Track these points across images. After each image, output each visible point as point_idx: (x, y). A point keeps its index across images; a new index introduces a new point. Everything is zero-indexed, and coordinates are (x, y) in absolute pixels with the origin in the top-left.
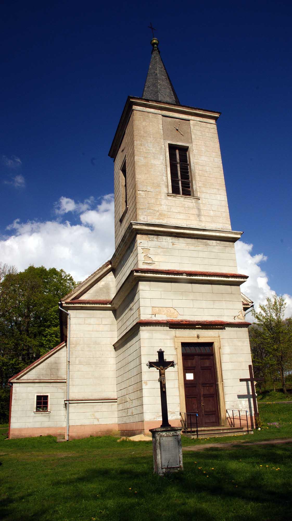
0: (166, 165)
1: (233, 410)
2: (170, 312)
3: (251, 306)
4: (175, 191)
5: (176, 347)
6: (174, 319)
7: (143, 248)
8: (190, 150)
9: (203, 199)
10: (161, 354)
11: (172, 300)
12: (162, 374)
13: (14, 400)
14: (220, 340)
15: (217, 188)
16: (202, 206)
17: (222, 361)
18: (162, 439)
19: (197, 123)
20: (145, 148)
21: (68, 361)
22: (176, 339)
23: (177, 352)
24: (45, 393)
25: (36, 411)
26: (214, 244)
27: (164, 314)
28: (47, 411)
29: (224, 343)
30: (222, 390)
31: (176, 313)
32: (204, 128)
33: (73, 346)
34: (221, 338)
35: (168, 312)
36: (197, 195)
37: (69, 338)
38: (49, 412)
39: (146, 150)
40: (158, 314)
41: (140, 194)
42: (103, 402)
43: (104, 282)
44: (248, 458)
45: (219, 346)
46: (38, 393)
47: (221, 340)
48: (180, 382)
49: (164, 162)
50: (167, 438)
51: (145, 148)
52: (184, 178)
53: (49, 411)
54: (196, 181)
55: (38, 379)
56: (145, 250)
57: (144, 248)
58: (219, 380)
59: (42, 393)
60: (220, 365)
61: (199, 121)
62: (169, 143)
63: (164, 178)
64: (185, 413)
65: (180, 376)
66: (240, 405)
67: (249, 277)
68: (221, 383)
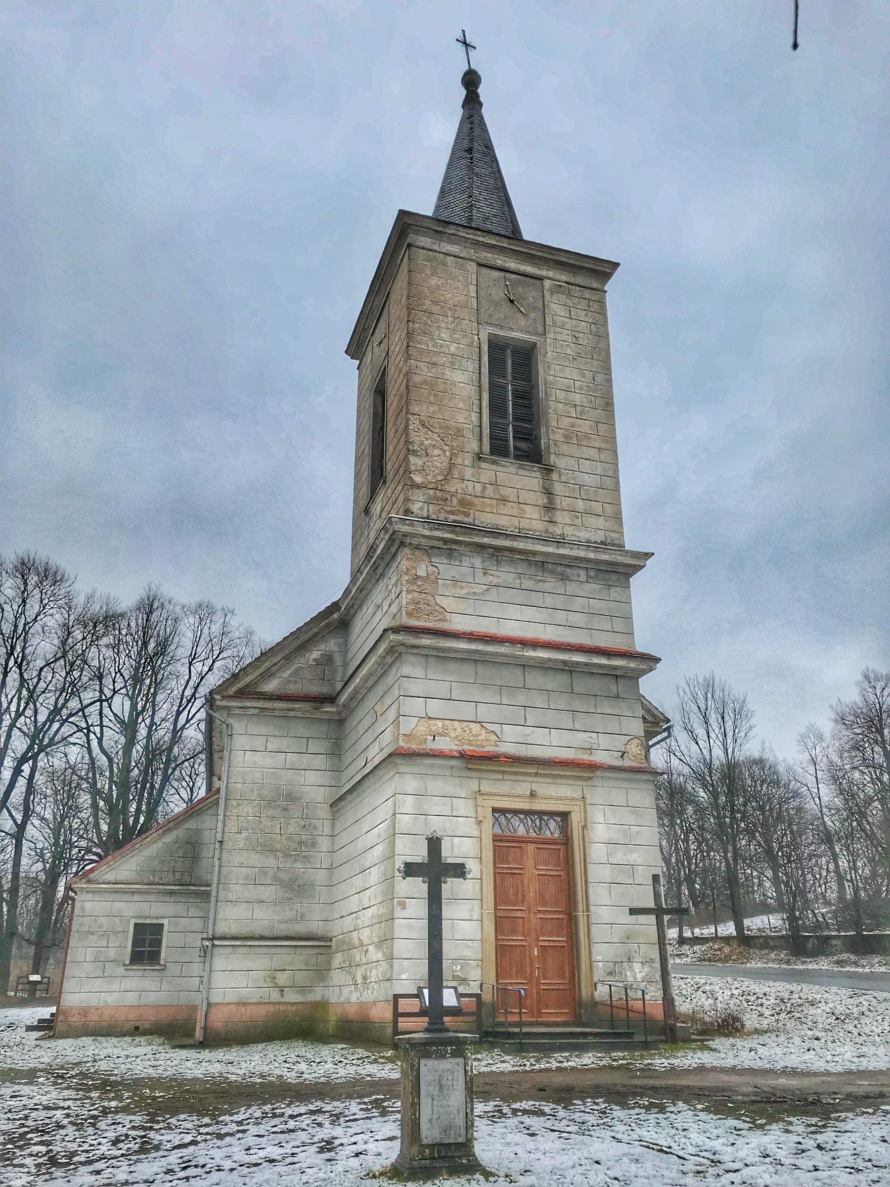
0: (480, 386)
1: (610, 986)
2: (471, 732)
3: (665, 730)
4: (499, 449)
5: (480, 818)
6: (478, 749)
8: (759, 930)
9: (562, 470)
10: (434, 844)
11: (501, 689)
12: (435, 901)
13: (76, 934)
14: (585, 807)
15: (596, 445)
16: (558, 488)
17: (588, 861)
19: (560, 286)
20: (433, 340)
22: (480, 798)
24: (157, 918)
26: (581, 579)
29: (598, 815)
32: (576, 301)
33: (234, 803)
34: (588, 802)
35: (465, 731)
36: (549, 461)
38: (162, 965)
39: (434, 346)
40: (441, 735)
41: (414, 451)
43: (319, 653)
46: (140, 917)
47: (588, 807)
48: (484, 906)
49: (475, 377)
51: (433, 340)
52: (526, 420)
53: (162, 962)
54: (547, 427)
59: (148, 917)
61: (566, 283)
62: (490, 331)
63: (474, 417)
64: (493, 986)
65: (485, 890)
66: (629, 973)
67: (660, 660)
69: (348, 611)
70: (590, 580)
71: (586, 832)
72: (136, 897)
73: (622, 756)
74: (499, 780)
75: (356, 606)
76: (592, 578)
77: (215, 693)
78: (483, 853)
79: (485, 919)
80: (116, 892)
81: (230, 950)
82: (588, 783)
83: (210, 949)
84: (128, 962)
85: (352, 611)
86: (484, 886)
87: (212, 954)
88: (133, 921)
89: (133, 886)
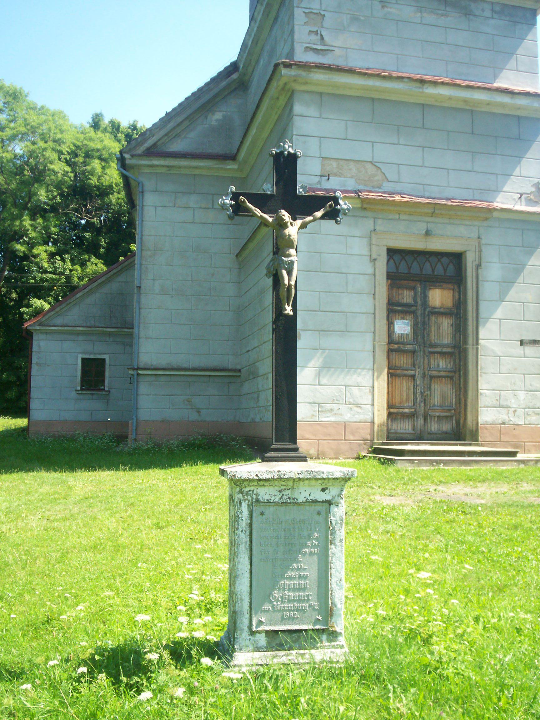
0: (374, 314)
5: (374, 256)
7: (307, 11)
17: (481, 298)
18: (262, 514)
21: (138, 287)
23: (375, 270)
25: (82, 389)
27: (349, 176)
28: (104, 390)
30: (475, 364)
31: (379, 177)
33: (149, 253)
34: (483, 242)
37: (140, 235)
40: (335, 175)
42: (210, 376)
44: (49, 157)
45: (477, 262)
46: (85, 353)
48: (377, 338)
50: (282, 509)
53: (107, 389)
55: (84, 325)
56: (312, 16)
57: (310, 11)
58: (470, 340)
60: (475, 306)
68: (475, 347)
69: (247, 70)
70: (495, 16)
71: (480, 271)
72: (81, 338)
73: (520, 198)
74: (394, 220)
75: (253, 63)
76: (497, 13)
77: (125, 152)
78: (377, 289)
79: (377, 350)
80: (64, 333)
81: (153, 378)
82: (485, 224)
83: (135, 377)
84: (79, 388)
85: (250, 69)
86: (377, 320)
87: (137, 382)
88: (80, 357)
89: (78, 328)
